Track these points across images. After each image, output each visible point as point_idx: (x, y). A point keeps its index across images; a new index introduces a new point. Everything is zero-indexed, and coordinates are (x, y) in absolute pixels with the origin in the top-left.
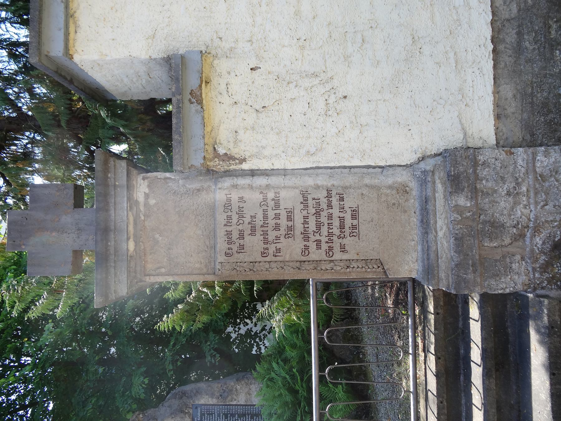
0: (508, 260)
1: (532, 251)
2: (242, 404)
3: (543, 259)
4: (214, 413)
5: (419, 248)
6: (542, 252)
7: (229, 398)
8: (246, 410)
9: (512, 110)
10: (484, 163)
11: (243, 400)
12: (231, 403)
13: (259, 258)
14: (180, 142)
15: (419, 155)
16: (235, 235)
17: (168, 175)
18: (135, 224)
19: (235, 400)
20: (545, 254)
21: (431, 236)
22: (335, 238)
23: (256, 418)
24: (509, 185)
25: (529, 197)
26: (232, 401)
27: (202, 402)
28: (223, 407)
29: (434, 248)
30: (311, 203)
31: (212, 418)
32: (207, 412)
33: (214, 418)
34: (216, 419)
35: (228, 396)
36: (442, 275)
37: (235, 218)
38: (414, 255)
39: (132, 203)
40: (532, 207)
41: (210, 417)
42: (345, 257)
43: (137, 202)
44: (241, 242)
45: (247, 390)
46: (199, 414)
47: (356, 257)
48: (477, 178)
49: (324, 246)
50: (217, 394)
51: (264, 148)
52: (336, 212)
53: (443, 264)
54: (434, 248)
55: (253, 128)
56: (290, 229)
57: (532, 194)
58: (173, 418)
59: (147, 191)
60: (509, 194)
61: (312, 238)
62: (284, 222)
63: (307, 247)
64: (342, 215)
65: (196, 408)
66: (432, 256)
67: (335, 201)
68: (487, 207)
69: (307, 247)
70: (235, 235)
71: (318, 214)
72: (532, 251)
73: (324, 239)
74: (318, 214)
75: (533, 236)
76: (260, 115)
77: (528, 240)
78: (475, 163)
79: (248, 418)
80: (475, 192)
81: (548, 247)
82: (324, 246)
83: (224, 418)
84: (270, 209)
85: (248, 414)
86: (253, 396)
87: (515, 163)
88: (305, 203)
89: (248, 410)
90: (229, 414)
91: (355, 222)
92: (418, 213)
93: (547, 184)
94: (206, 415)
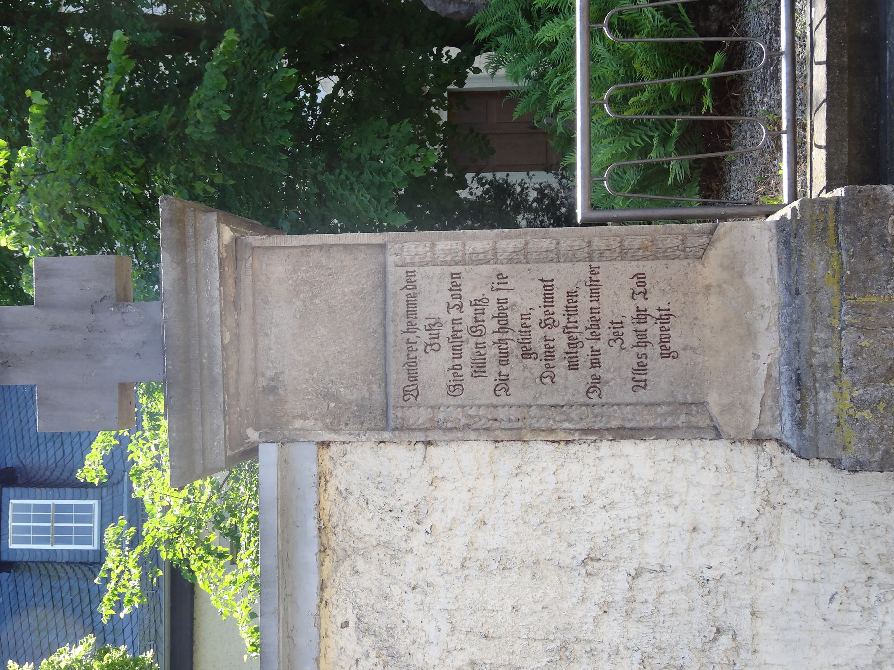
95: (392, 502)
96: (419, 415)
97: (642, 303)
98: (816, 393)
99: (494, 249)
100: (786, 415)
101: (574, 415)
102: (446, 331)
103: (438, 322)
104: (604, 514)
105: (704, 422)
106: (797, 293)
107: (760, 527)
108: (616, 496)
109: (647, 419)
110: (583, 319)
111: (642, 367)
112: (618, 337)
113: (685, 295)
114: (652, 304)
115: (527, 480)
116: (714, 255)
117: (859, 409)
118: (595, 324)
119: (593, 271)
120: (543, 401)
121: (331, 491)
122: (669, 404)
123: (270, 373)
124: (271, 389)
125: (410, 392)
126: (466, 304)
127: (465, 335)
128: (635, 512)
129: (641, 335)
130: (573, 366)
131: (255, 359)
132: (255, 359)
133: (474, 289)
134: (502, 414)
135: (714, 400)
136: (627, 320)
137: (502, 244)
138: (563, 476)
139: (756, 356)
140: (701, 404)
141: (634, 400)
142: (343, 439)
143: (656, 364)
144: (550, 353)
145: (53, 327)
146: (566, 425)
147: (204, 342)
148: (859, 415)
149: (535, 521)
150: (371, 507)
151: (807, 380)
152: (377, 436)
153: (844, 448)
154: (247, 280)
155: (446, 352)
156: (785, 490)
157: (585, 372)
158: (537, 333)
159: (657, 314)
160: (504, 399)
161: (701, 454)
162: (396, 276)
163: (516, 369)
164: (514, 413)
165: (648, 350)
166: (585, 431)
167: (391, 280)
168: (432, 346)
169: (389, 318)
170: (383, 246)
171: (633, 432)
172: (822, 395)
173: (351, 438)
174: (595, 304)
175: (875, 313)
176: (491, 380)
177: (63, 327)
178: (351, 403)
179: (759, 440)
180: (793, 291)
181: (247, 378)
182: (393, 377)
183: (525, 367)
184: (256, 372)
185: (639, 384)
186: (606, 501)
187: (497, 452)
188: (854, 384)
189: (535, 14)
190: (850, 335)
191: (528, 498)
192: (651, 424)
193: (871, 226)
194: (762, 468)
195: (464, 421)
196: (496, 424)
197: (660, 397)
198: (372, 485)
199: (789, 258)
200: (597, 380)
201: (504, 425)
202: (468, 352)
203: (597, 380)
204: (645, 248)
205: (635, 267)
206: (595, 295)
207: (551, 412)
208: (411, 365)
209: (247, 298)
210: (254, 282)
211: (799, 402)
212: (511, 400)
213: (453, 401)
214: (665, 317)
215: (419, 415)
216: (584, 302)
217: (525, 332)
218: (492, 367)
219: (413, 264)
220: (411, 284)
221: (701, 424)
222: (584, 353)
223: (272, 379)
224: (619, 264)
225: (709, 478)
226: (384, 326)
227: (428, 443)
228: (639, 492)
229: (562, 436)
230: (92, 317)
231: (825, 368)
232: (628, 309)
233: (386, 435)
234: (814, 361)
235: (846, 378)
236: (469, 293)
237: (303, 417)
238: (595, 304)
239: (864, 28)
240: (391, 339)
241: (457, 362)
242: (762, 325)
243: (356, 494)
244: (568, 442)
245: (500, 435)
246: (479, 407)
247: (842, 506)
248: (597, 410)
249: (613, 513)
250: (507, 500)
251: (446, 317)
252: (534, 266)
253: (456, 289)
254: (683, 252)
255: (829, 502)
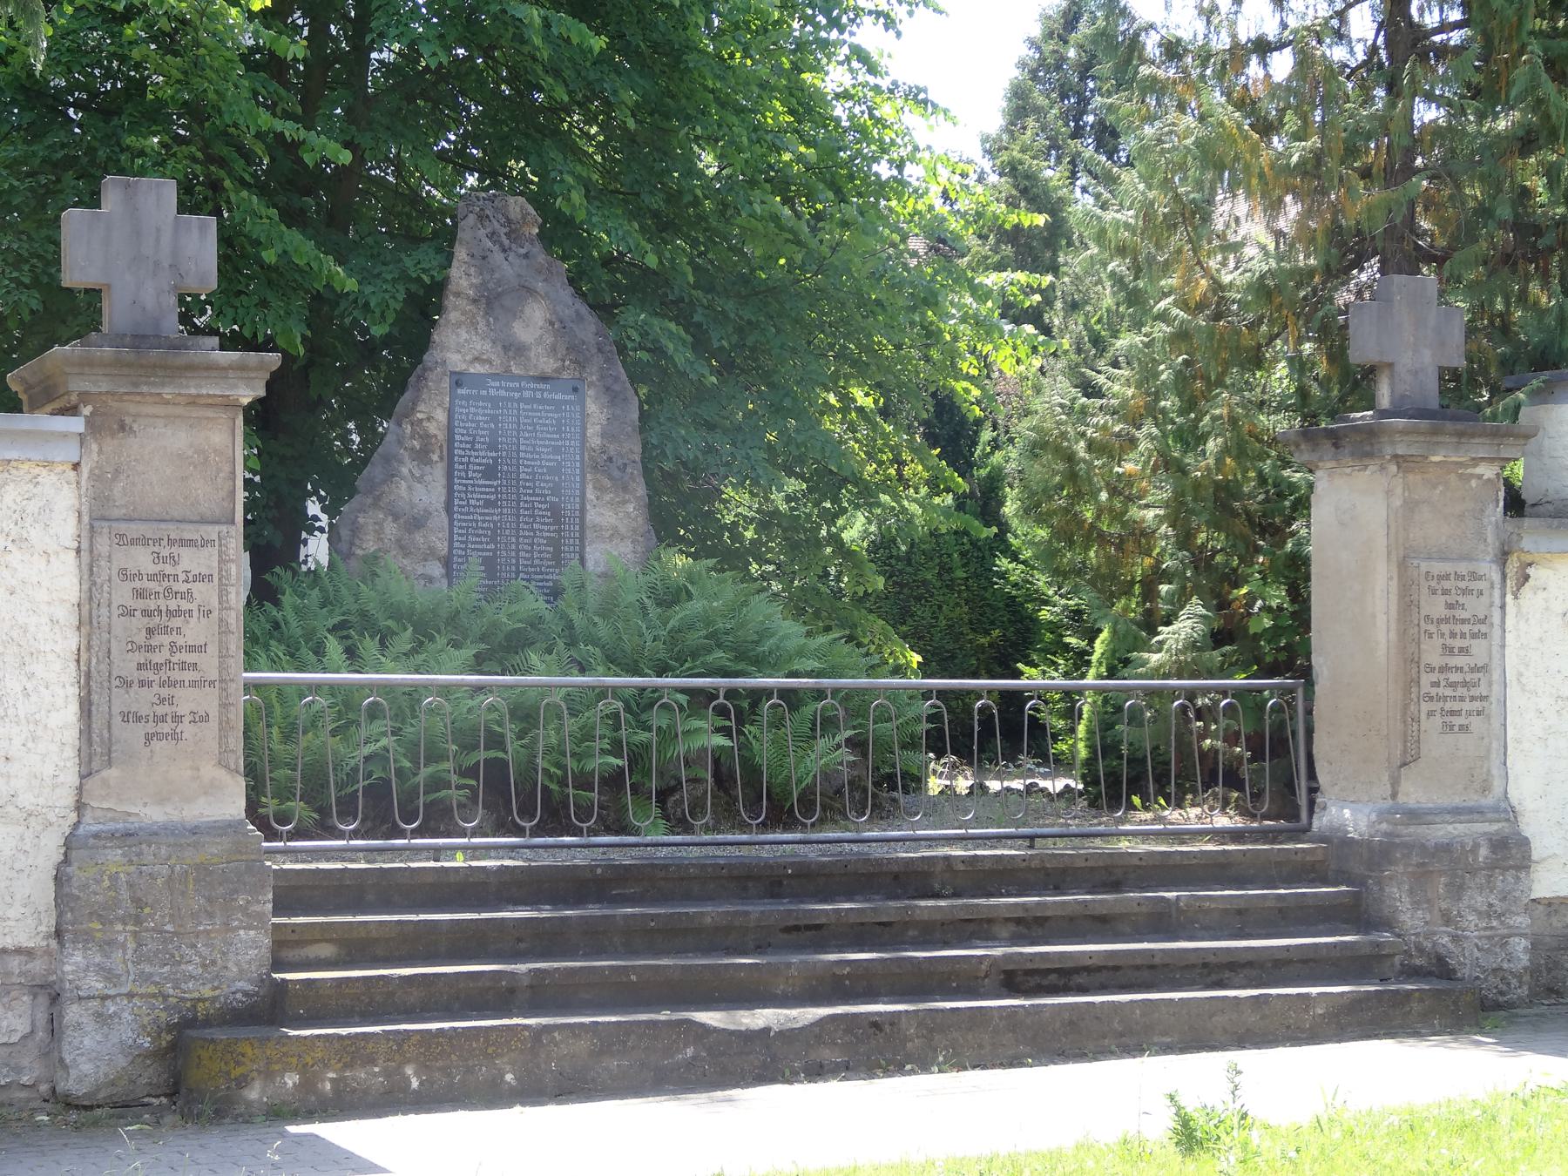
0: (1425, 906)
1: (1435, 933)
2: (588, 517)
3: (1428, 945)
5: (1431, 805)
6: (1434, 944)
7: (607, 483)
9: (1554, 924)
10: (1518, 878)
11: (598, 520)
12: (590, 487)
13: (1423, 613)
14: (1550, 527)
15: (1518, 808)
16: (1446, 584)
17: (1502, 504)
18: (1457, 463)
20: (1434, 946)
21: (1448, 817)
22: (1441, 704)
23: (548, 552)
24: (1499, 906)
25: (1486, 929)
27: (592, 407)
28: (578, 464)
29: (1437, 820)
30: (1476, 676)
31: (548, 432)
32: (566, 419)
35: (611, 478)
36: (1412, 829)
37: (1462, 585)
38: (1423, 800)
39: (1476, 461)
40: (1476, 933)
41: (552, 426)
42: (1423, 716)
43: (1475, 466)
44: (1439, 592)
45: (623, 530)
46: (559, 396)
47: (1423, 729)
48: (1506, 869)
49: (1434, 691)
50: (612, 449)
51: (1527, 620)
52: (1467, 706)
53: (1422, 830)
54: (1437, 820)
55: (1547, 609)
56: (1451, 650)
57: (1488, 933)
58: (551, 323)
59: (1485, 477)
60: (1490, 905)
61: (1442, 677)
62: (1458, 643)
63: (1433, 670)
64: (1464, 713)
65: (575, 390)
66: (1430, 818)
67: (1477, 705)
68: (1477, 880)
69: (1433, 670)
70: (1446, 584)
71: (1465, 684)
72: (1435, 933)
73: (1441, 691)
74: (1465, 684)
75: (1449, 934)
76: (1560, 618)
77: (1444, 929)
78: (1519, 868)
79: (549, 531)
80: (1492, 866)
81: (1442, 951)
82: (1434, 691)
84: (1470, 626)
85: (559, 531)
86: (608, 547)
87: (1518, 914)
88: (1475, 669)
90: (560, 478)
91: (1456, 729)
92: (1465, 804)
93: (1498, 950)
94: (556, 416)
95: (29, 520)
96: (103, 544)
97: (186, 720)
98: (120, 848)
99: (230, 608)
100: (101, 826)
101: (103, 667)
102: (168, 569)
103: (176, 563)
104: (19, 688)
105: (95, 765)
106: (195, 834)
107: (10, 809)
108: (34, 698)
109: (98, 723)
110: (176, 675)
111: (138, 719)
112: (162, 701)
113: (192, 752)
114: (187, 728)
115: (47, 629)
116: (222, 774)
117: (110, 878)
118: (172, 684)
119: (212, 683)
120: (114, 644)
121: (37, 470)
122: (110, 739)
123: (135, 427)
124: (122, 427)
125: (122, 540)
126: (189, 586)
127: (165, 584)
128: (21, 713)
129: (163, 719)
130: (140, 666)
131: (147, 416)
132: (147, 416)
133: (201, 592)
134: (104, 611)
135: (112, 774)
136: (174, 708)
137: (233, 614)
138: (51, 657)
139: (145, 805)
140: (110, 764)
141: (113, 713)
142: (83, 483)
143: (139, 730)
144: (150, 649)
145: (158, 230)
146: (94, 660)
147: (167, 380)
148: (105, 878)
149: (14, 634)
150: (25, 502)
151: (130, 841)
152: (85, 509)
153: (80, 868)
154: (210, 413)
155: (153, 569)
156: (39, 828)
157: (136, 675)
158: (165, 640)
159: (178, 731)
160: (116, 612)
161: (68, 764)
162: (212, 532)
163: (138, 622)
164: (104, 620)
165: (151, 724)
166: (88, 675)
167: (209, 528)
168: (158, 558)
169: (178, 524)
170: (233, 522)
171: (86, 713)
172: (120, 852)
173: (83, 490)
174: (187, 684)
175: (182, 887)
176: (131, 603)
177: (158, 240)
178: (111, 490)
179: (80, 807)
180: (195, 831)
181: (132, 408)
182: (133, 526)
183: (140, 630)
184: (136, 416)
185: (125, 717)
186: (29, 691)
187: (69, 605)
188: (128, 874)
189: (345, 633)
190: (165, 870)
191: (32, 629)
192: (94, 726)
193: (244, 884)
194: (57, 810)
195: (99, 581)
196: (95, 606)
197: (115, 731)
198: (41, 504)
199: (220, 828)
200: (129, 684)
201: (95, 612)
202: (153, 586)
203: (129, 684)
204: (228, 722)
205: (214, 713)
206: (193, 684)
207: (105, 648)
208: (143, 541)
209: (196, 412)
210: (208, 418)
211: (113, 835)
212: (115, 617)
213: (114, 572)
214: (175, 736)
215: (103, 544)
216: (189, 676)
217: (167, 630)
218: (140, 604)
219: (220, 545)
220: (205, 543)
221: (93, 763)
222: (149, 675)
223: (131, 428)
224: (216, 703)
225: (49, 770)
226: (171, 520)
227: (78, 551)
228: (37, 717)
229: (84, 656)
230: (166, 265)
231: (139, 854)
232: (183, 709)
233: (86, 519)
234: (144, 846)
235: (133, 868)
236: (197, 588)
237: (100, 452)
238: (187, 684)
239: (370, 897)
240: (163, 526)
241: (145, 577)
242: (169, 809)
243: (35, 491)
244: (78, 661)
245: (85, 609)
246: (110, 593)
247: (27, 872)
248: (106, 684)
249: (20, 696)
250: (31, 613)
251: (179, 570)
252: (216, 638)
253: (200, 578)
254: (224, 750)
255: (30, 862)
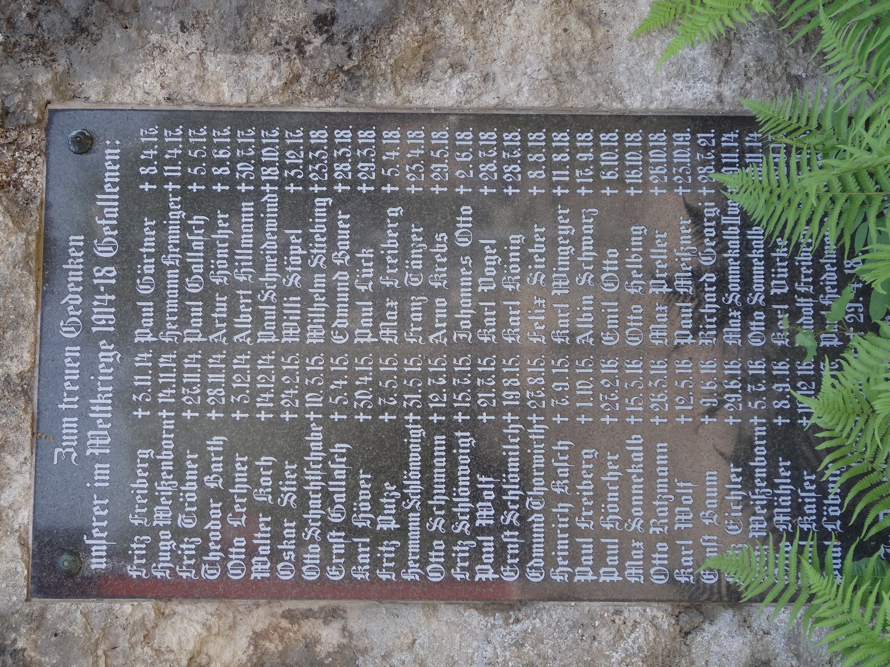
4: (257, 195)
8: (550, 166)
19: (458, 67)
26: (422, 77)
28: (343, 135)
32: (185, 180)
33: (247, 240)
34: (271, 245)
79: (576, 241)
83: (344, 233)
85: (575, 204)
89: (574, 164)
